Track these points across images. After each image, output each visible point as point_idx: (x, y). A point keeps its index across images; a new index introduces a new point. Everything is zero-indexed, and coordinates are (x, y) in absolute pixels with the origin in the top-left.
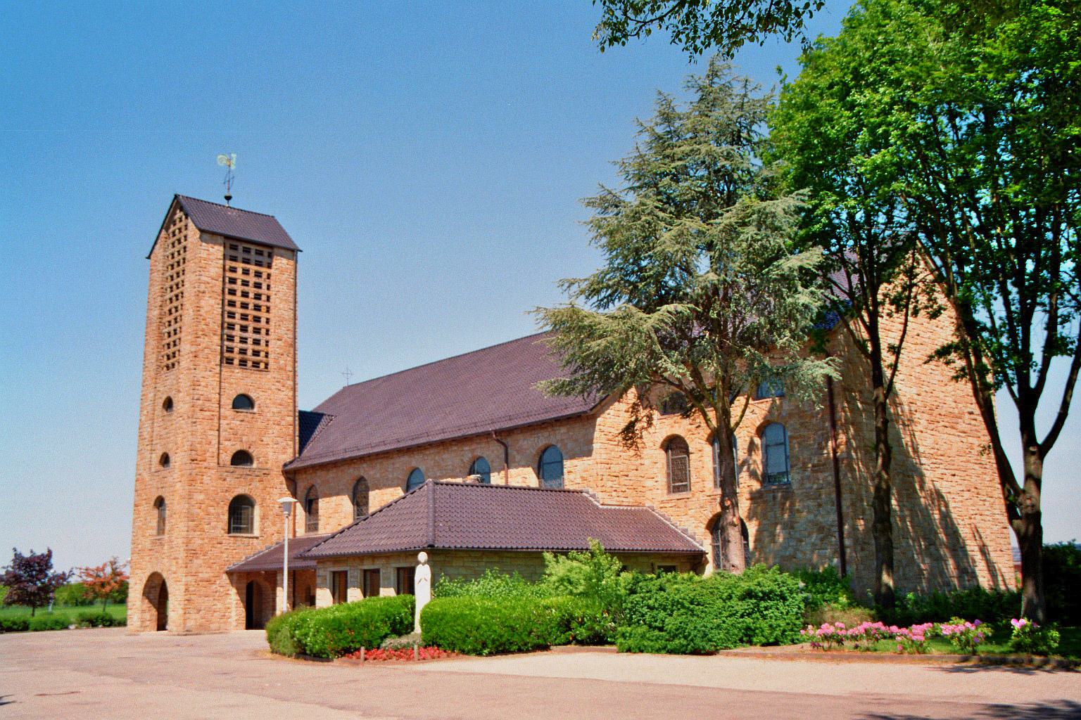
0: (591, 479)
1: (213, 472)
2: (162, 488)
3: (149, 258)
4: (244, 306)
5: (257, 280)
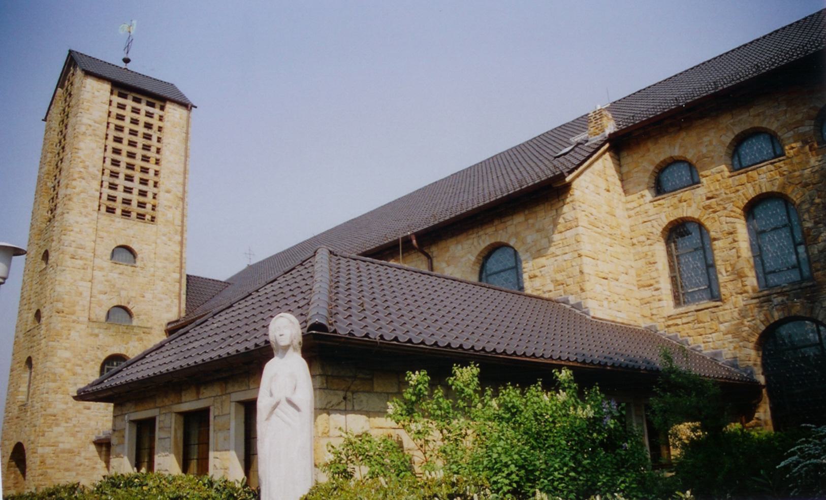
0: (570, 281)
1: (84, 327)
2: (31, 347)
3: (45, 120)
4: (131, 155)
5: (146, 131)
